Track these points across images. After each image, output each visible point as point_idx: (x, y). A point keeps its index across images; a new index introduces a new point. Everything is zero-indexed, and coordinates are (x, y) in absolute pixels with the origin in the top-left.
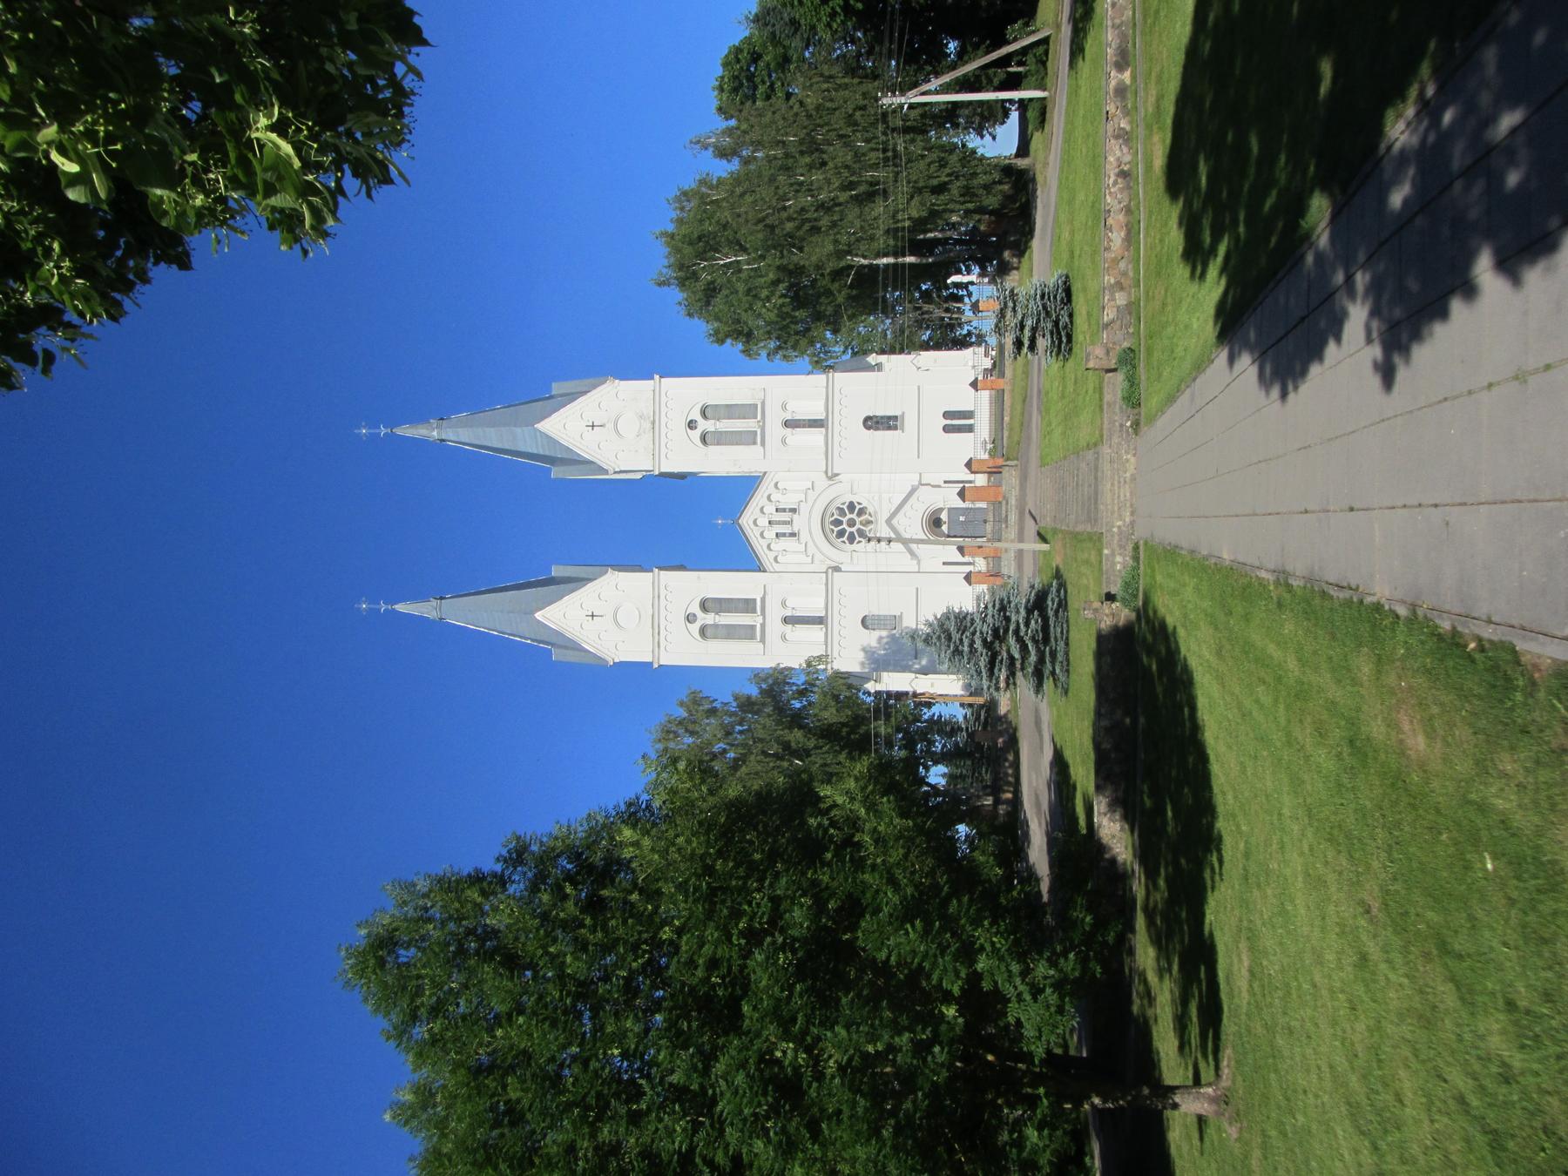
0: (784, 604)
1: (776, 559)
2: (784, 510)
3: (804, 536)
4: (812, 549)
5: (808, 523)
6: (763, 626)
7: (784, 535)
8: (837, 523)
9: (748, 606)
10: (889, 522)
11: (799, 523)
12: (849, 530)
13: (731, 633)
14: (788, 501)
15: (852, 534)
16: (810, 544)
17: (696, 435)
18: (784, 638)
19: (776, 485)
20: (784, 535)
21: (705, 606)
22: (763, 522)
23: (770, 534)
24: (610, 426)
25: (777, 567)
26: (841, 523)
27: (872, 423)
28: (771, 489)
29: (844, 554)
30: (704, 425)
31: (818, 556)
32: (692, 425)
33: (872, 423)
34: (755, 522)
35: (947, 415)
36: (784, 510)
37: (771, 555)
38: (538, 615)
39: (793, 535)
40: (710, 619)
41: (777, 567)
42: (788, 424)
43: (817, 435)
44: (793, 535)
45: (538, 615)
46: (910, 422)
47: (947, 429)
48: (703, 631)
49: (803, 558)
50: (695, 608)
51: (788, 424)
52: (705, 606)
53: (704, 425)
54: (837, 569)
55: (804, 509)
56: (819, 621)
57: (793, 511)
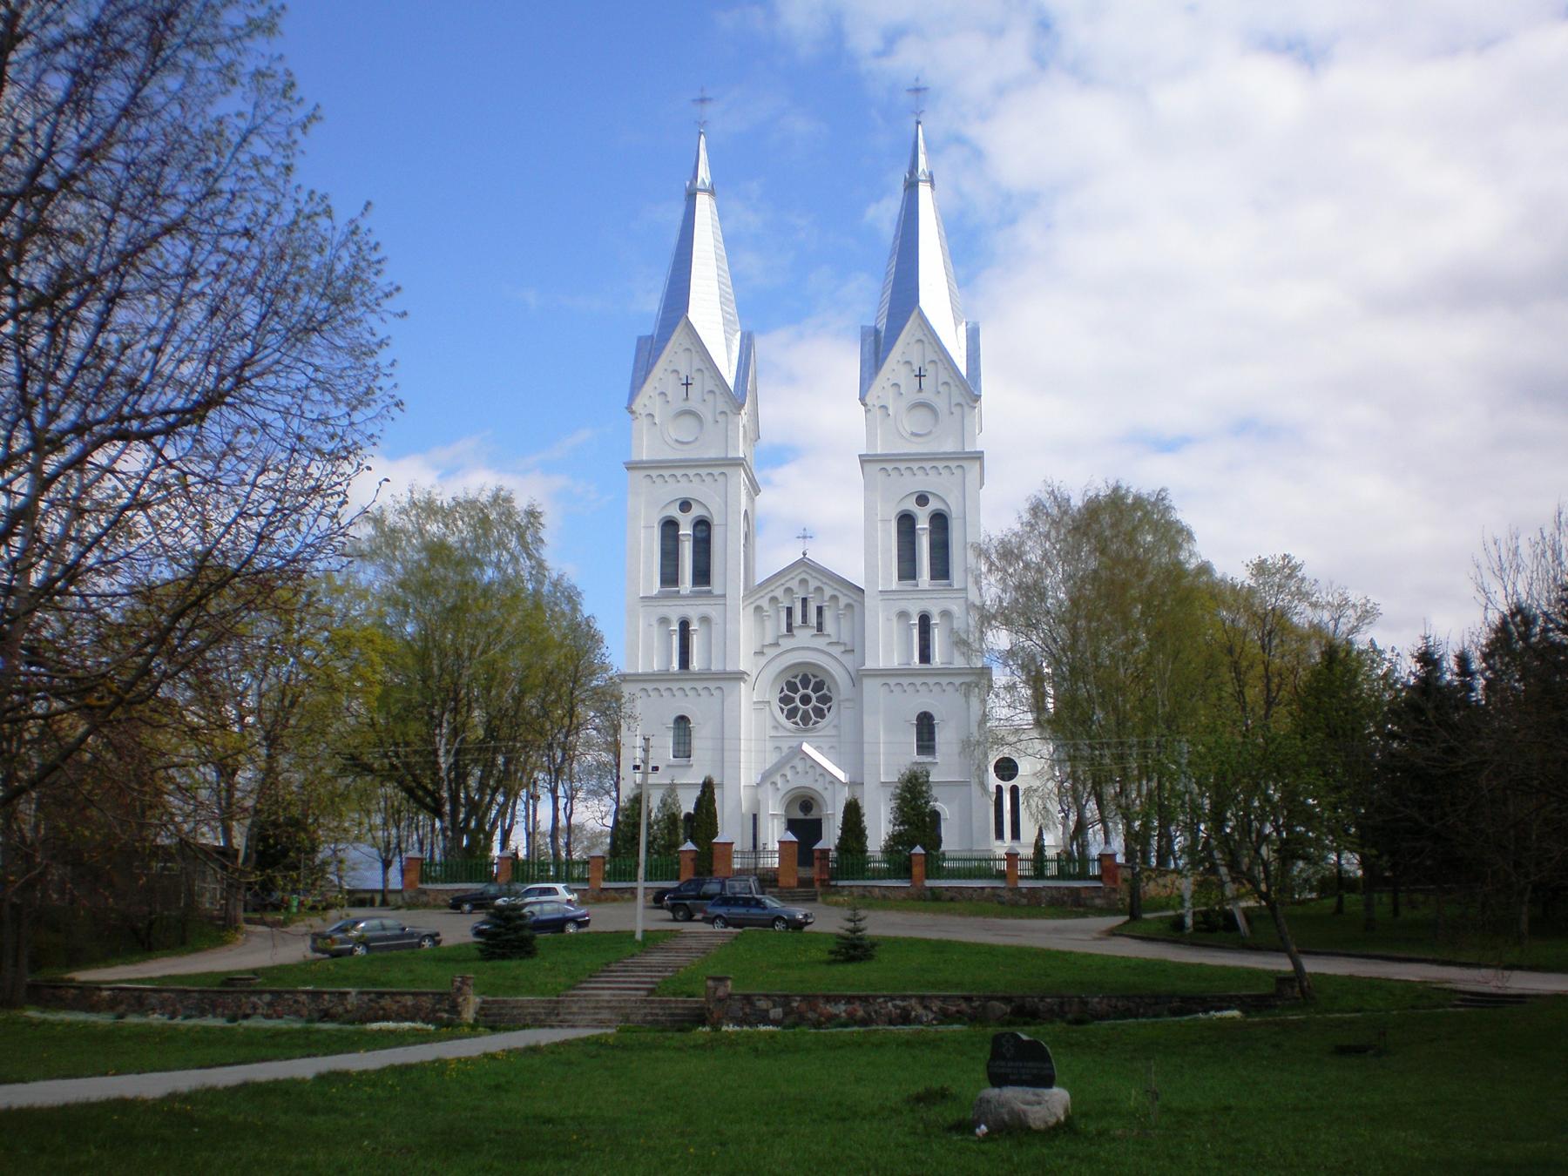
3: (787, 643)
4: (771, 652)
44: (790, 628)
51: (684, 625)
55: (820, 642)
56: (925, 656)
57: (820, 627)
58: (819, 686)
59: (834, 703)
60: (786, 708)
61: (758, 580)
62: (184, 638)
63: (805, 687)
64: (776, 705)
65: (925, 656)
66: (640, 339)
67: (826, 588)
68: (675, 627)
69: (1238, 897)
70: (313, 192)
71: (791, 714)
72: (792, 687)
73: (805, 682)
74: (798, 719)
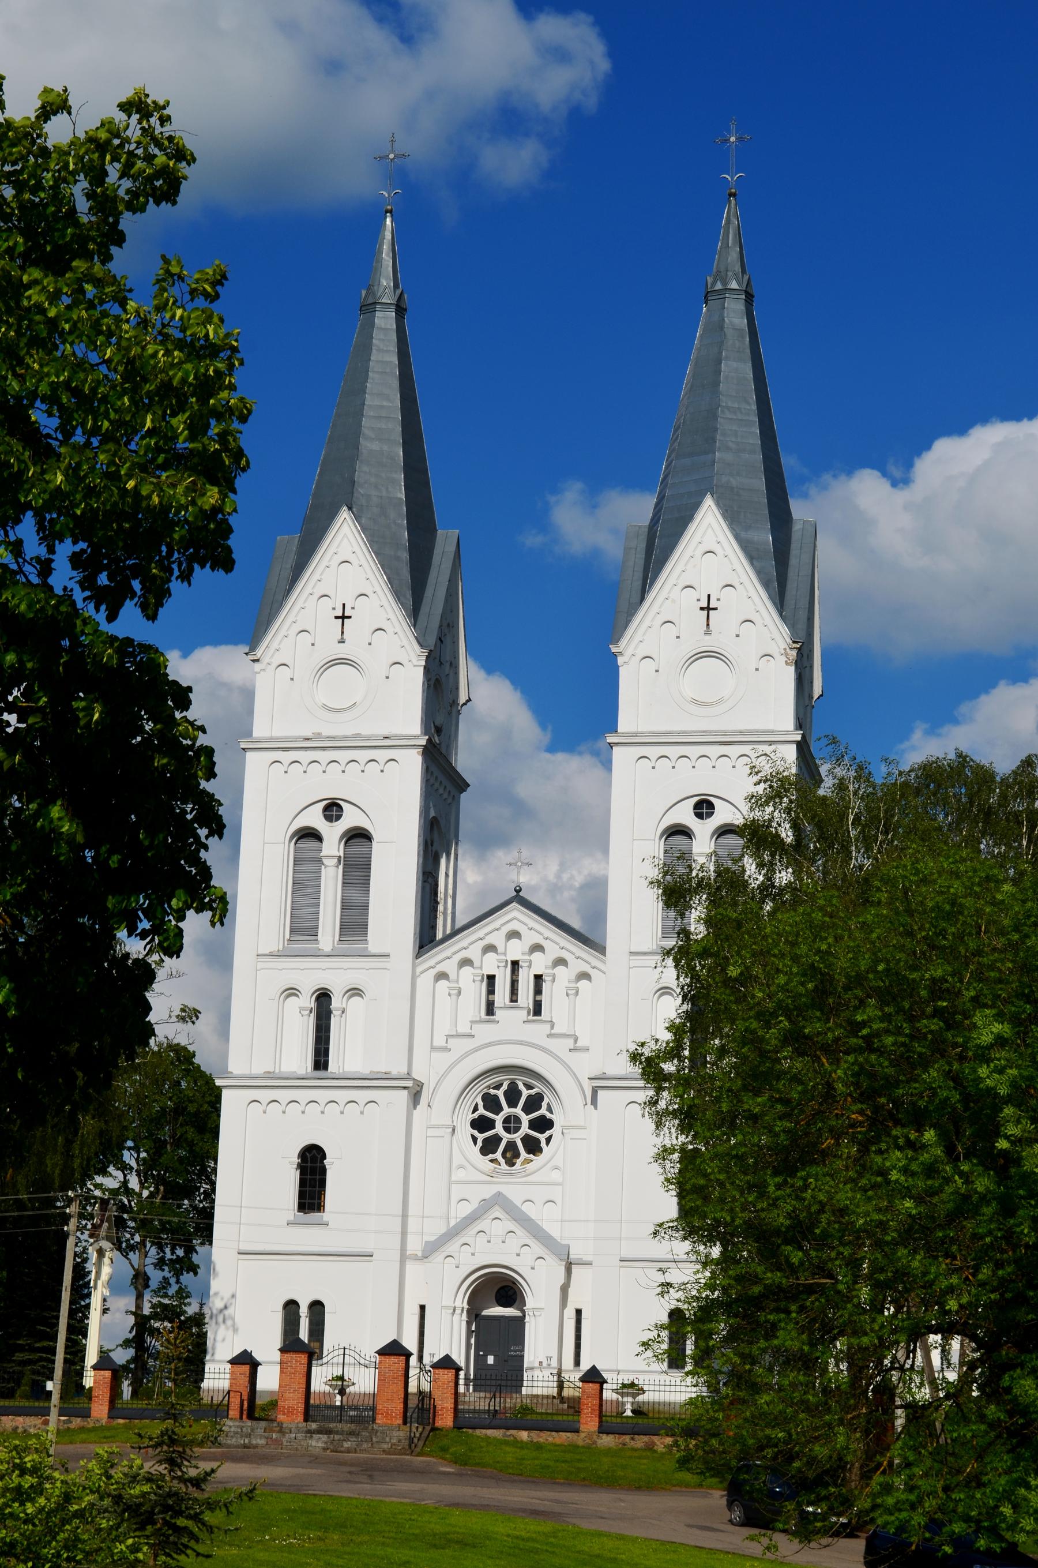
0: (355, 992)
1: (442, 976)
2: (538, 991)
3: (486, 1032)
4: (460, 1046)
5: (508, 1039)
6: (317, 955)
7: (491, 991)
8: (513, 1096)
9: (354, 922)
10: (499, 1200)
11: (512, 1020)
12: (499, 1119)
13: (304, 887)
14: (553, 995)
15: (533, 1125)
16: (468, 1044)
17: (685, 815)
18: (292, 992)
19: (584, 976)
20: (491, 991)
21: (358, 836)
22: (516, 950)
23: (491, 964)
24: (342, 651)
25: (426, 981)
26: (512, 1102)
27: (312, 1165)
28: (577, 965)
29: (449, 1113)
30: (332, 833)
31: (448, 1058)
32: (333, 810)
33: (312, 1165)
34: (514, 935)
35: (317, 1307)
36: (538, 991)
37: (450, 967)
38: (709, 502)
39: (490, 1009)
40: (332, 845)
41: (426, 981)
42: (323, 997)
43: (298, 1056)
44: (490, 1009)
45: (709, 502)
46: (309, 1236)
47: (291, 1307)
48: (309, 834)
49: (443, 1027)
50: (350, 819)
51: (323, 997)
52: (358, 836)
53: (332, 833)
54: (416, 1096)
55: (537, 1031)
56: (321, 1061)
57: (537, 1009)
58: (534, 1103)
59: (555, 1131)
60: (481, 1137)
61: (457, 927)
62: (1001, 989)
63: (512, 1104)
64: (466, 1131)
65: (321, 1061)
66: (227, 573)
67: (490, 940)
68: (309, 1002)
69: (135, 1549)
70: (241, 433)
71: (489, 1147)
72: (491, 1103)
73: (513, 1096)
74: (498, 1155)
